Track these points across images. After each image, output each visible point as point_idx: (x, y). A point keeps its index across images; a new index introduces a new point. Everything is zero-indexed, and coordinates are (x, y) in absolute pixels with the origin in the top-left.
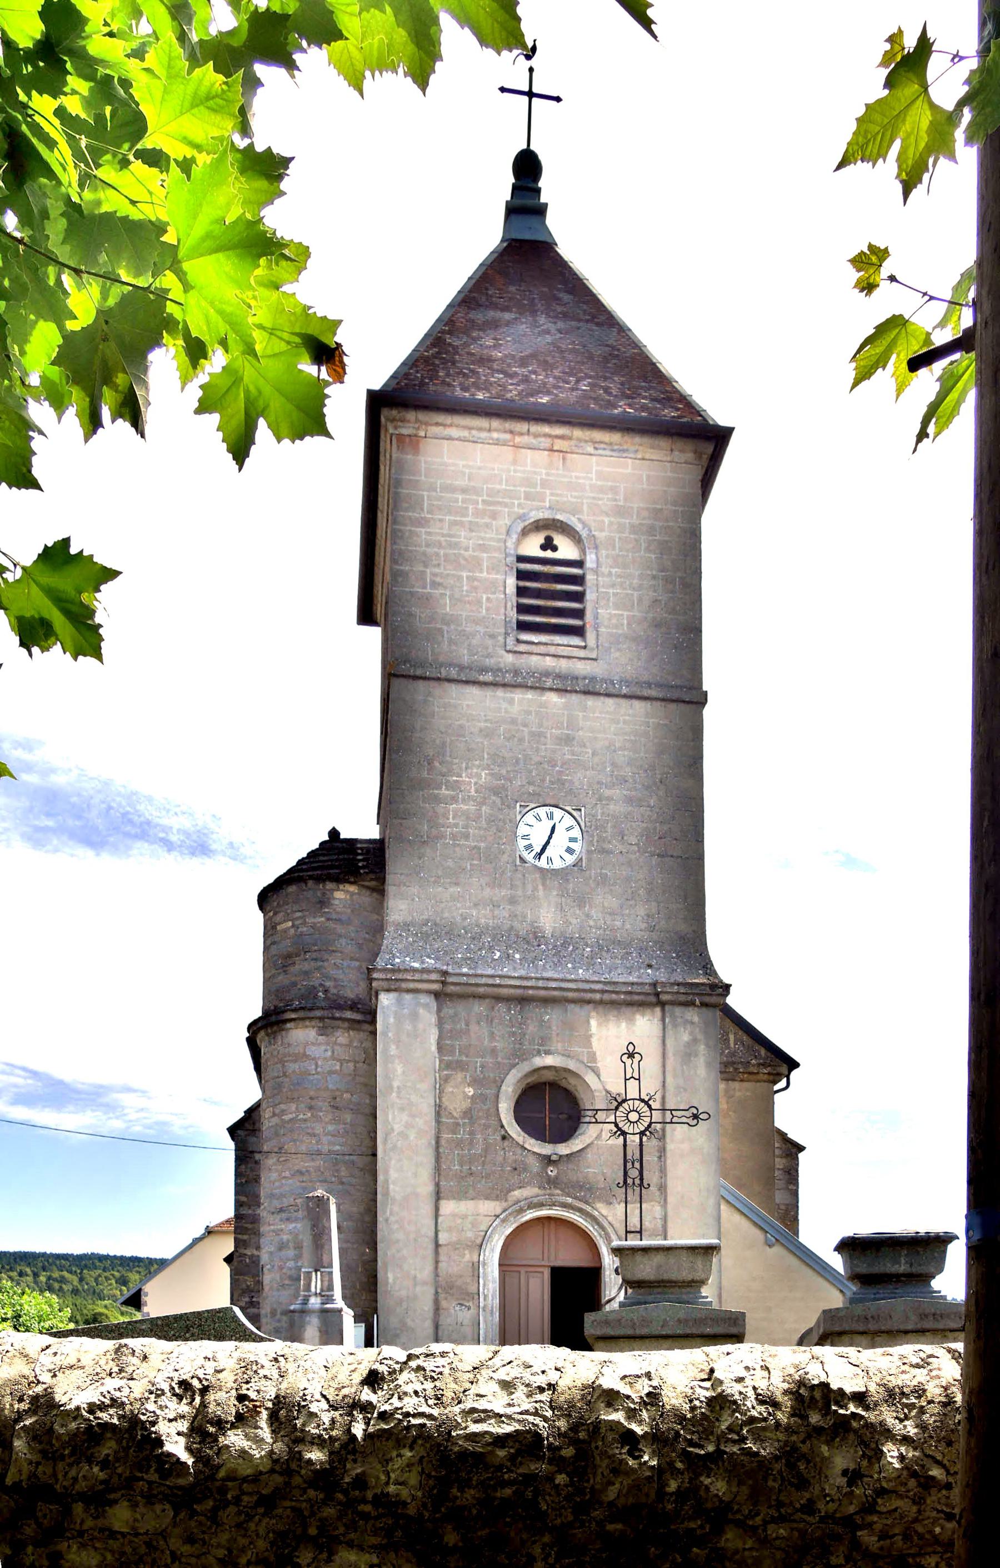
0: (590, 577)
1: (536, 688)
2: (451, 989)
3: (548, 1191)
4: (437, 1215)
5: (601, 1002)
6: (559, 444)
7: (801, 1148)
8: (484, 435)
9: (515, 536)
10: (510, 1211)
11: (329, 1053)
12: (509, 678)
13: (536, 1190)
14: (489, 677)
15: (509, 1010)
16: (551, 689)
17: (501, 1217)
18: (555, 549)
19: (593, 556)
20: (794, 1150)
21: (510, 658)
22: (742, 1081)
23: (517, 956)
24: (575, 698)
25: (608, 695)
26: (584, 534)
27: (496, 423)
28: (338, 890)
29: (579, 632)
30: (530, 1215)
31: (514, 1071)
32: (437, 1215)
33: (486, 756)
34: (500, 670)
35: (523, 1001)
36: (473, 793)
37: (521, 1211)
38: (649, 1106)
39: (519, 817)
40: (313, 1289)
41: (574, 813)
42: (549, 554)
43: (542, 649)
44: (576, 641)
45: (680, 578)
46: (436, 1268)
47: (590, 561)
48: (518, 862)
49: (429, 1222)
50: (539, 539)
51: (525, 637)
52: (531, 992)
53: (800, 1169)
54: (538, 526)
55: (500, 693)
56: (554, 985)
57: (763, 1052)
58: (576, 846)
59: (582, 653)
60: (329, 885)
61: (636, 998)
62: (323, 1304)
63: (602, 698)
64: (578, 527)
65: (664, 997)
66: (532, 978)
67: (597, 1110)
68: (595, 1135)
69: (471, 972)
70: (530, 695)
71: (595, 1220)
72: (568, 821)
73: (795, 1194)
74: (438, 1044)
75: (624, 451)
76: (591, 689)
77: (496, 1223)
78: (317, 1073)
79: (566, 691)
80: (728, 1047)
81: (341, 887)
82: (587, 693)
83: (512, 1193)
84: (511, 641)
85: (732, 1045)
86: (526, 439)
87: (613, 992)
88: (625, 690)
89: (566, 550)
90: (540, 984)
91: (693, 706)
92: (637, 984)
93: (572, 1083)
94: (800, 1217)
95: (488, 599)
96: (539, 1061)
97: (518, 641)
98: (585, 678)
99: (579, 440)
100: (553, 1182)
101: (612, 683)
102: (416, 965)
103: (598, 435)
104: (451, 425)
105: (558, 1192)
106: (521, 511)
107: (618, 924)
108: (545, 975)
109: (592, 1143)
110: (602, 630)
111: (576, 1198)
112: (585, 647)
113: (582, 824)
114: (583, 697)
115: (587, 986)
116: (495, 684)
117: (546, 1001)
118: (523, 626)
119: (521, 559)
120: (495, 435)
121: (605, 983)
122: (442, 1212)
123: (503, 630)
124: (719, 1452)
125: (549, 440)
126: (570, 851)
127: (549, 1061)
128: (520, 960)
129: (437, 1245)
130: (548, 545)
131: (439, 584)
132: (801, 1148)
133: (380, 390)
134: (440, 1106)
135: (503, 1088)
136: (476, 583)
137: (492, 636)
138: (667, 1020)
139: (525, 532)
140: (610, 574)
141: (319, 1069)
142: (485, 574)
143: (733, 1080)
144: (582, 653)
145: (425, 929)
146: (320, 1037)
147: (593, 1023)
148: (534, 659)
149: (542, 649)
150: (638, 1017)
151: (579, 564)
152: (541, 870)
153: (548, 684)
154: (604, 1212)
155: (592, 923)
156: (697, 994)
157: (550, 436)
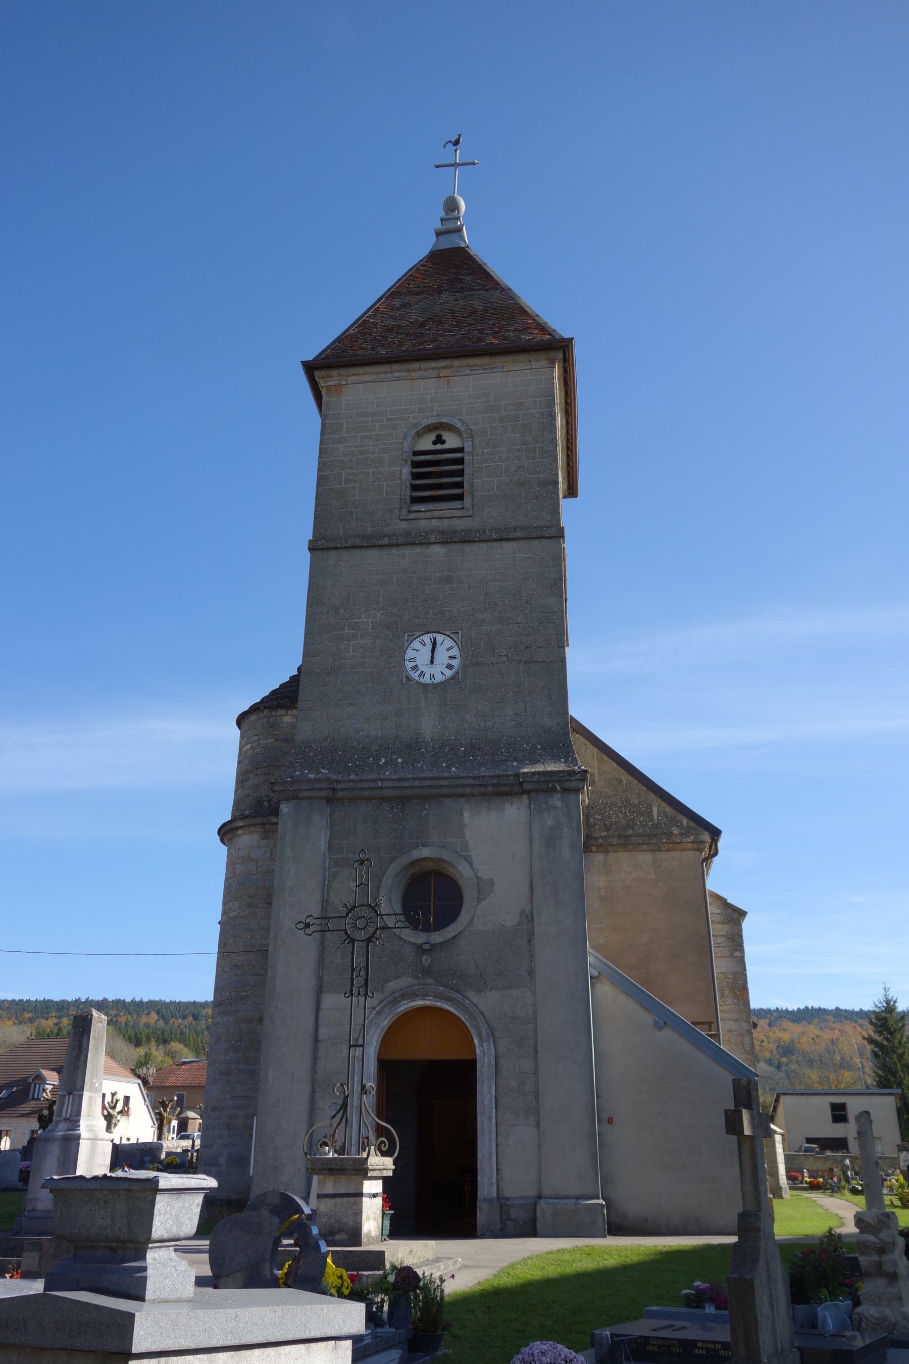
0: (467, 458)
1: (423, 544)
2: (340, 794)
3: (421, 981)
4: (318, 1009)
5: (473, 795)
6: (443, 373)
7: (743, 914)
8: (388, 376)
9: (410, 439)
10: (386, 1001)
11: (268, 854)
12: (401, 539)
13: (410, 980)
14: (386, 541)
15: (392, 808)
16: (435, 543)
17: (377, 1009)
18: (443, 442)
19: (470, 443)
20: (736, 916)
21: (403, 525)
22: (668, 850)
23: (400, 760)
24: (455, 547)
25: (482, 541)
26: (463, 429)
27: (396, 367)
28: (287, 715)
29: (460, 497)
30: (404, 1006)
31: (394, 865)
32: (318, 1009)
33: (381, 600)
34: (395, 535)
35: (403, 800)
36: (370, 630)
37: (395, 1002)
38: (376, 912)
39: (406, 645)
40: (64, 1114)
41: (453, 636)
42: (439, 447)
43: (429, 514)
44: (457, 504)
45: (540, 447)
46: (314, 1065)
47: (468, 447)
48: (404, 681)
49: (309, 1018)
50: (432, 437)
51: (416, 507)
52: (408, 791)
53: (744, 934)
54: (429, 429)
55: (394, 551)
56: (428, 783)
57: (685, 821)
58: (455, 663)
59: (460, 513)
60: (281, 712)
61: (503, 789)
62: (68, 1130)
63: (477, 544)
64: (459, 425)
65: (527, 786)
66: (408, 779)
67: (330, 918)
68: (466, 922)
69: (357, 778)
70: (418, 550)
71: (466, 1010)
72: (449, 642)
73: (741, 961)
74: (329, 844)
75: (493, 368)
76: (467, 539)
77: (372, 1015)
78: (257, 873)
79: (448, 543)
80: (652, 819)
81: (289, 712)
82: (464, 542)
83: (389, 984)
84: (404, 513)
85: (656, 817)
86: (419, 373)
87: (481, 785)
88: (494, 536)
89: (451, 441)
90: (416, 783)
91: (552, 541)
92: (503, 776)
93: (451, 871)
94: (749, 986)
95: (388, 485)
96: (417, 854)
97: (410, 512)
98: (463, 531)
99: (459, 367)
100: (427, 972)
101: (484, 531)
102: (312, 776)
103: (471, 361)
104: (364, 374)
105: (431, 981)
106: (415, 421)
107: (489, 724)
108: (423, 775)
109: (464, 930)
110: (477, 493)
111: (447, 986)
112: (463, 508)
113: (460, 644)
114: (461, 545)
115: (458, 782)
116: (390, 546)
117: (425, 798)
118: (415, 500)
119: (416, 453)
120: (396, 375)
121: (475, 778)
122: (323, 1006)
123: (398, 506)
124: (411, 1308)
125: (437, 371)
126: (449, 667)
127: (425, 852)
128: (402, 763)
129: (316, 1040)
130: (439, 440)
131: (351, 480)
132: (743, 914)
133: (313, 360)
134: (327, 901)
135: (384, 880)
136: (379, 476)
137: (390, 511)
138: (532, 807)
139: (419, 434)
140: (483, 453)
141: (259, 870)
142: (386, 469)
143: (659, 850)
144: (460, 513)
145: (324, 744)
146: (262, 841)
147: (466, 814)
148: (423, 522)
149: (429, 514)
150: (507, 805)
151: (461, 450)
152: (425, 686)
153: (432, 540)
154: (475, 1000)
155: (466, 725)
156: (558, 781)
157: (436, 368)
